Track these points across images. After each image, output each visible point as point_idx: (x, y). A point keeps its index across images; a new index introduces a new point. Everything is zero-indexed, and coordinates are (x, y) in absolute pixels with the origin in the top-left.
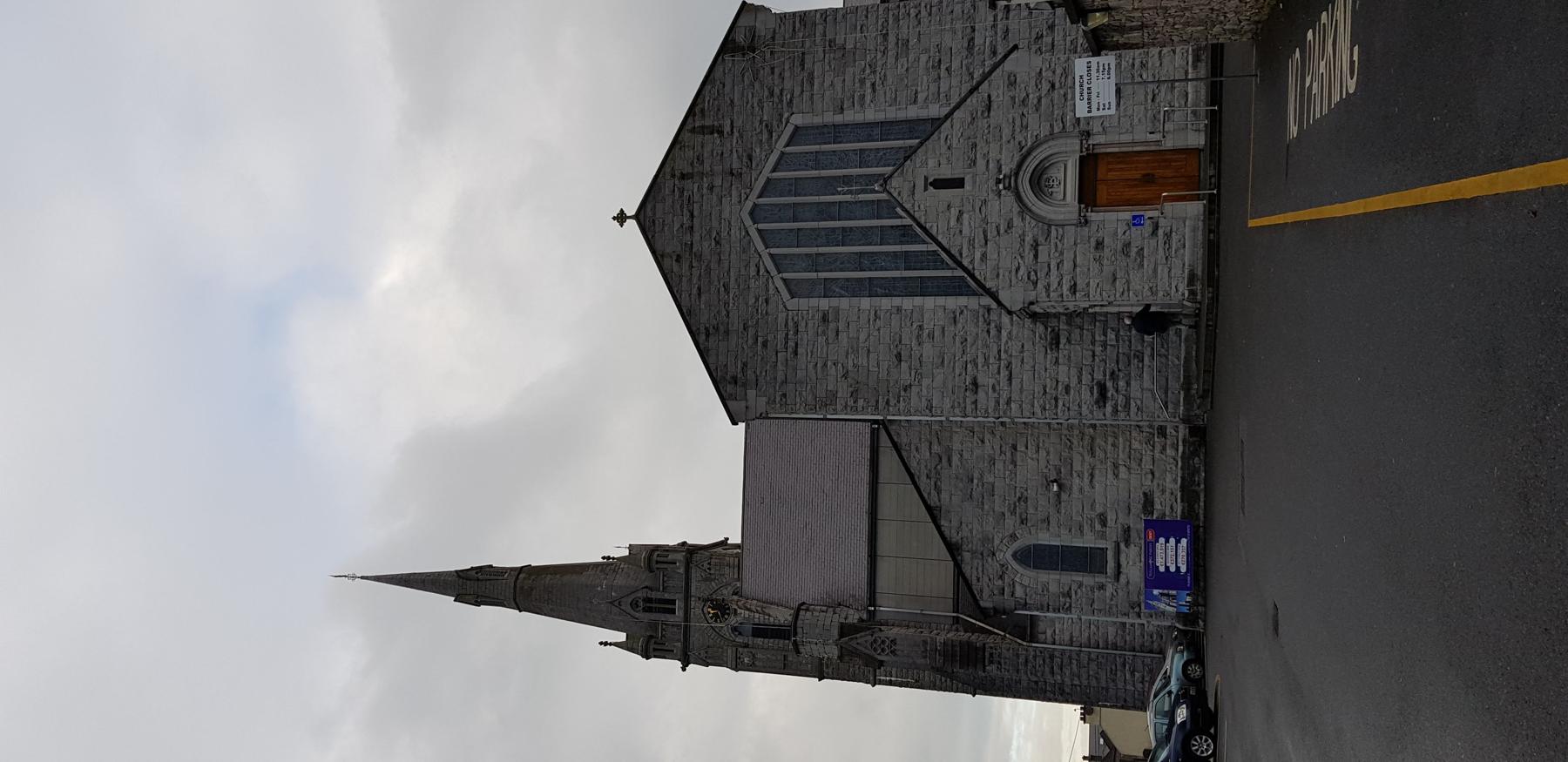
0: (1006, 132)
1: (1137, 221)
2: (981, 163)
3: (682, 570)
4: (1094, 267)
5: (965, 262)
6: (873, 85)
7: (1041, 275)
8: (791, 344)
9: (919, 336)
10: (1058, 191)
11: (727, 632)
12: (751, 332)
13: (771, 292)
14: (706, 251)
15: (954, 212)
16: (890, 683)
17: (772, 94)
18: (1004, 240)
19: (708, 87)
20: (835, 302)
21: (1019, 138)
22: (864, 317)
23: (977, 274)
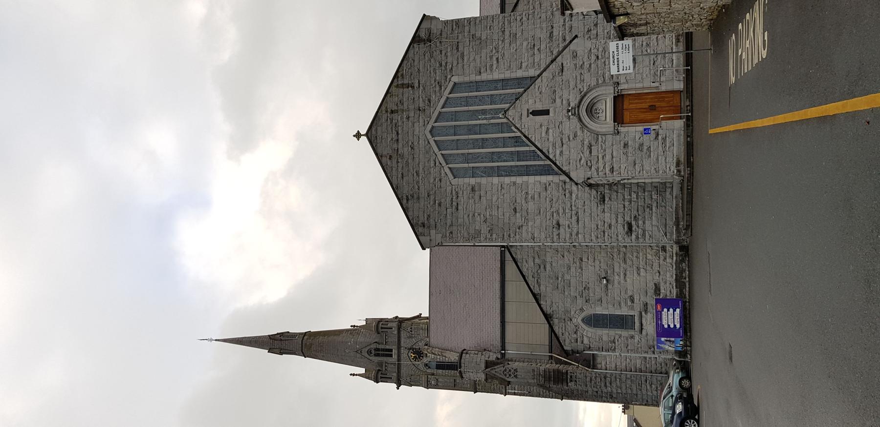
0: (572, 84)
1: (646, 131)
2: (558, 101)
3: (396, 332)
4: (623, 158)
5: (551, 157)
6: (497, 59)
7: (594, 162)
8: (455, 204)
9: (526, 198)
10: (602, 116)
11: (421, 367)
12: (432, 197)
13: (443, 175)
14: (406, 153)
15: (544, 129)
16: (515, 394)
17: (441, 65)
18: (572, 144)
19: (405, 62)
20: (478, 180)
21: (579, 86)
22: (495, 187)
23: (558, 163)
